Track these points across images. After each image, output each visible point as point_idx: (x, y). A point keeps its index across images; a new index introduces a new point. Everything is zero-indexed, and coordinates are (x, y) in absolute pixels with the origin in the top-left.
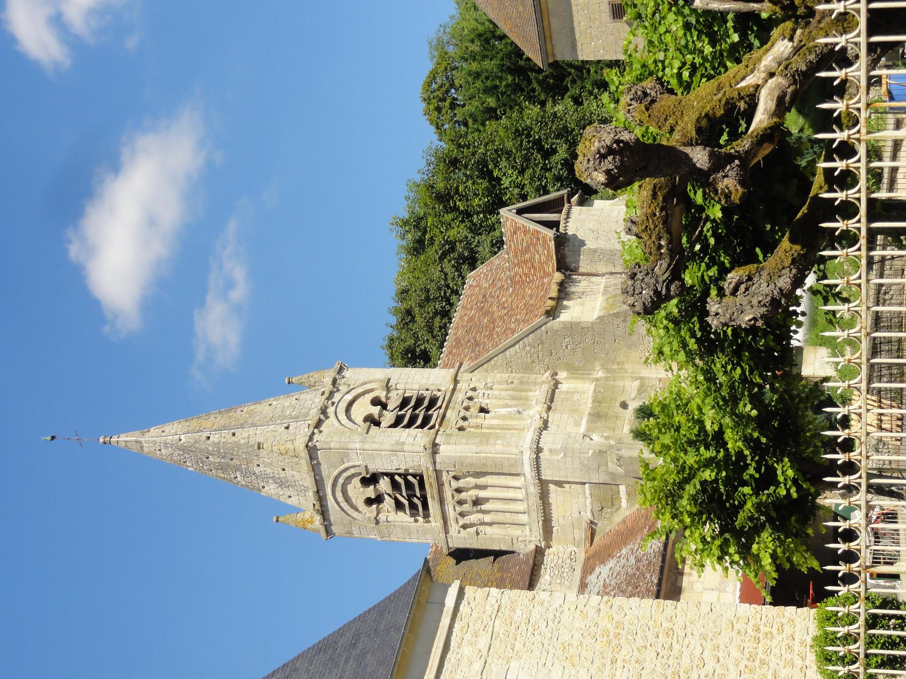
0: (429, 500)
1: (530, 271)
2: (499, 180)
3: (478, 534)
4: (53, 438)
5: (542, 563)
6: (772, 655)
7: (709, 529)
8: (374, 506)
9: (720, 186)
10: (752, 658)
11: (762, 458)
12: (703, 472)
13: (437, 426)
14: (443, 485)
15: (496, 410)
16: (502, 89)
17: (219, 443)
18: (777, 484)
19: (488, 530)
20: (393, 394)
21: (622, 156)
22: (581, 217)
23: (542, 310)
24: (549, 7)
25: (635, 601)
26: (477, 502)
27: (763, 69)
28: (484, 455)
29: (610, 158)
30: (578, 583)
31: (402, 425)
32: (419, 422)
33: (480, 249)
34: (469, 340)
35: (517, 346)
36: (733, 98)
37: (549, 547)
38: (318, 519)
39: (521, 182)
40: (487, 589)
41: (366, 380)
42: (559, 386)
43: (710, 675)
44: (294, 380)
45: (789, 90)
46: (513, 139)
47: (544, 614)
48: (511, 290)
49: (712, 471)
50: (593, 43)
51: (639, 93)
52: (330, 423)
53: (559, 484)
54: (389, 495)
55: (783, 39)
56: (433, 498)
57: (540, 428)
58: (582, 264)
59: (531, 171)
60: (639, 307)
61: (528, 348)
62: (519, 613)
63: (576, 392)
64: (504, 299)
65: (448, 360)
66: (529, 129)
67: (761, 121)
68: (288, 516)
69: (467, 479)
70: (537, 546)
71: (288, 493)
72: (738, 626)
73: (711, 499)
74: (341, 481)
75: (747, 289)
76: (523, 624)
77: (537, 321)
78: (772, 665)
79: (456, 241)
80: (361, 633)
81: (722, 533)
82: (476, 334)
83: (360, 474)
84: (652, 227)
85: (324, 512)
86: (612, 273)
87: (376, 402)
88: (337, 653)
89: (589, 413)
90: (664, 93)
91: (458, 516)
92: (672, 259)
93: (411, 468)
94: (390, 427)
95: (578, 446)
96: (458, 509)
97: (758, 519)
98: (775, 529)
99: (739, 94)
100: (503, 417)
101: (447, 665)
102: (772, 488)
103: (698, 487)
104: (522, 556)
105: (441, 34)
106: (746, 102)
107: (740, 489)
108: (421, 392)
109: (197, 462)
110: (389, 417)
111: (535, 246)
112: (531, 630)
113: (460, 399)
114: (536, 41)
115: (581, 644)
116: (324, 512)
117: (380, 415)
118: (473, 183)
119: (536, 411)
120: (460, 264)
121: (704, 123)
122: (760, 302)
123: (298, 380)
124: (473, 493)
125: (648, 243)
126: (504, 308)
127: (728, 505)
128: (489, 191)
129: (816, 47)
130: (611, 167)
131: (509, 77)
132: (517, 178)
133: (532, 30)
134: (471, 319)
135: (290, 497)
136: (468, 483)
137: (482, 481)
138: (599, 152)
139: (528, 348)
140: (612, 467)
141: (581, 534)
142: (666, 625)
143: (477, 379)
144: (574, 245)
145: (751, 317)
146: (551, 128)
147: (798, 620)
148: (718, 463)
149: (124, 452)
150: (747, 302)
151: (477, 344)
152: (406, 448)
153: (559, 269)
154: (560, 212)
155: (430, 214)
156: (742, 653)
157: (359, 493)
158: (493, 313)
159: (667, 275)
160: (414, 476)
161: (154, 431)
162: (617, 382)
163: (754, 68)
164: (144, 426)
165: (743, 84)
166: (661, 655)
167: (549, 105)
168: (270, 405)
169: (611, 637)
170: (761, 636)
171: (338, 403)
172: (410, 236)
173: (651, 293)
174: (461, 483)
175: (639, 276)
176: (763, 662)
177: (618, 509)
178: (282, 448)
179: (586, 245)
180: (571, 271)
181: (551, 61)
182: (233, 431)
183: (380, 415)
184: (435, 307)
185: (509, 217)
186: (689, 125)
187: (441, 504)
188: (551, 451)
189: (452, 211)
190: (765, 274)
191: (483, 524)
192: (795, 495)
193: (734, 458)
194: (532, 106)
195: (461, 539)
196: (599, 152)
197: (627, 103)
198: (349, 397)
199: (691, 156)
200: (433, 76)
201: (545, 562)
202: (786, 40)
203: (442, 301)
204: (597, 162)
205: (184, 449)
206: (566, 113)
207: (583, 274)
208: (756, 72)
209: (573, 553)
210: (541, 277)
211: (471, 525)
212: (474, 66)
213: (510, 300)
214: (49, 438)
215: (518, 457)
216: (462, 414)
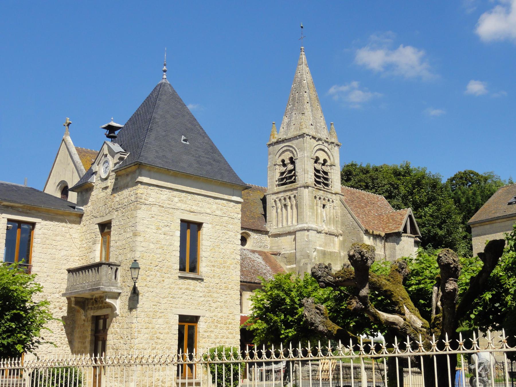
0: (285, 186)
1: (386, 222)
2: (427, 206)
3: (273, 207)
4: (302, 27)
5: (262, 234)
6: (220, 330)
7: (267, 303)
8: (281, 163)
9: (353, 301)
10: (218, 322)
11: (296, 322)
12: (289, 299)
13: (316, 187)
14: (292, 191)
15: (324, 211)
16: (469, 205)
17: (304, 97)
18: (285, 329)
19: (275, 211)
20: (329, 168)
21: (361, 261)
22: (409, 243)
23: (368, 228)
24: (494, 224)
25: (239, 273)
26: (285, 206)
27: (411, 316)
28: (305, 207)
29: (360, 256)
30: (255, 249)
31: (316, 173)
32: (317, 180)
33: (395, 200)
34: (354, 198)
35: (352, 219)
36: (399, 304)
37: (269, 237)
38: (275, 140)
39: (427, 216)
40: (240, 213)
41: (334, 156)
42: (336, 237)
43: (210, 305)
44: (332, 126)
45: (398, 327)
46: (445, 211)
47: (232, 237)
48: (377, 214)
49: (290, 302)
50: (479, 244)
51: (403, 266)
52: (314, 142)
53: (295, 239)
54: (286, 170)
55: (422, 324)
56: (286, 187)
57: (317, 230)
58: (389, 244)
59: (432, 220)
60: (314, 270)
61: (351, 223)
62: (231, 226)
63: (334, 244)
64: (372, 212)
65: (345, 190)
66: (451, 217)
67: (383, 316)
68: (275, 128)
69: (295, 201)
70: (269, 232)
71: (285, 127)
72: (231, 316)
73: (279, 302)
74: (291, 149)
75: (317, 313)
76: (227, 228)
77: (363, 226)
78: (216, 330)
79: (398, 189)
80: (219, 163)
81: (265, 307)
82: (357, 201)
83: (294, 157)
84: (346, 274)
85: (278, 142)
86: (386, 256)
87: (325, 161)
88: (211, 154)
89: (325, 250)
90: (403, 276)
91: (279, 198)
92: (334, 283)
93: (298, 178)
94: (315, 168)
95: (311, 246)
96: (282, 198)
97: (271, 322)
98: (268, 329)
99: (401, 307)
100: (321, 214)
101: (208, 199)
102: (284, 327)
103: (283, 297)
104: (265, 226)
105: (495, 177)
106: (398, 309)
107: (283, 314)
108: (330, 179)
109: (295, 88)
110: (319, 167)
111: (396, 223)
112: (225, 232)
113: (328, 196)
114: (479, 219)
115: (220, 253)
116: (278, 142)
117: (319, 163)
118: (425, 195)
119: (325, 228)
120: (388, 192)
121: (389, 293)
122: (312, 318)
123: (332, 128)
124: (289, 204)
125: (340, 273)
126: (368, 212)
127: (277, 309)
128: (422, 202)
129: (417, 337)
130: (356, 257)
131: (474, 208)
132: (429, 214)
133: (483, 217)
134: (363, 199)
135: (283, 128)
136: (293, 202)
137: (294, 207)
138: (362, 252)
139: (351, 223)
140: (303, 261)
141: (275, 250)
142: (230, 286)
143: (337, 202)
144: (397, 240)
145: (307, 315)
146: (451, 227)
147: (235, 340)
148: (292, 305)
149: (298, 58)
150: (312, 313)
151: (352, 202)
152: (306, 175)
153: (386, 234)
154: (411, 233)
155: (411, 177)
156: (220, 318)
157: (286, 156)
158: (366, 207)
159: (327, 281)
160: (295, 179)
161: (307, 69)
162: (339, 261)
163: (412, 312)
164: (310, 64)
165: (405, 308)
166: (217, 285)
167: (462, 225)
168: (321, 117)
169: (223, 264)
170: (227, 325)
171: (323, 145)
172: (402, 169)
173: (320, 275)
174: (293, 199)
175: (326, 270)
176: (216, 326)
177: (286, 264)
178: (303, 123)
179: (397, 245)
180: (386, 240)
181: (471, 226)
182: (309, 102)
183: (319, 163)
184: (370, 182)
185: (407, 212)
186: (388, 287)
187: (284, 191)
188: (308, 235)
189: (413, 187)
190: (324, 320)
191: (277, 210)
192: (281, 337)
193: (295, 311)
194: (461, 218)
195: (270, 200)
196: (362, 252)
197: (399, 261)
198: (326, 149)
199: (364, 288)
200: (477, 175)
201: (262, 235)
202: (422, 325)
203: (373, 185)
204: (358, 251)
205: (300, 82)
206: (458, 233)
207: (384, 244)
208: (410, 313)
209: (267, 247)
210: (382, 227)
211: (276, 204)
212: (478, 192)
213: (372, 214)
214: (302, 26)
215: (305, 222)
216: (322, 197)
